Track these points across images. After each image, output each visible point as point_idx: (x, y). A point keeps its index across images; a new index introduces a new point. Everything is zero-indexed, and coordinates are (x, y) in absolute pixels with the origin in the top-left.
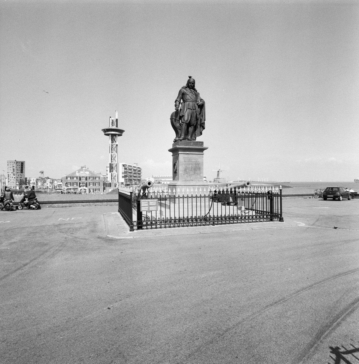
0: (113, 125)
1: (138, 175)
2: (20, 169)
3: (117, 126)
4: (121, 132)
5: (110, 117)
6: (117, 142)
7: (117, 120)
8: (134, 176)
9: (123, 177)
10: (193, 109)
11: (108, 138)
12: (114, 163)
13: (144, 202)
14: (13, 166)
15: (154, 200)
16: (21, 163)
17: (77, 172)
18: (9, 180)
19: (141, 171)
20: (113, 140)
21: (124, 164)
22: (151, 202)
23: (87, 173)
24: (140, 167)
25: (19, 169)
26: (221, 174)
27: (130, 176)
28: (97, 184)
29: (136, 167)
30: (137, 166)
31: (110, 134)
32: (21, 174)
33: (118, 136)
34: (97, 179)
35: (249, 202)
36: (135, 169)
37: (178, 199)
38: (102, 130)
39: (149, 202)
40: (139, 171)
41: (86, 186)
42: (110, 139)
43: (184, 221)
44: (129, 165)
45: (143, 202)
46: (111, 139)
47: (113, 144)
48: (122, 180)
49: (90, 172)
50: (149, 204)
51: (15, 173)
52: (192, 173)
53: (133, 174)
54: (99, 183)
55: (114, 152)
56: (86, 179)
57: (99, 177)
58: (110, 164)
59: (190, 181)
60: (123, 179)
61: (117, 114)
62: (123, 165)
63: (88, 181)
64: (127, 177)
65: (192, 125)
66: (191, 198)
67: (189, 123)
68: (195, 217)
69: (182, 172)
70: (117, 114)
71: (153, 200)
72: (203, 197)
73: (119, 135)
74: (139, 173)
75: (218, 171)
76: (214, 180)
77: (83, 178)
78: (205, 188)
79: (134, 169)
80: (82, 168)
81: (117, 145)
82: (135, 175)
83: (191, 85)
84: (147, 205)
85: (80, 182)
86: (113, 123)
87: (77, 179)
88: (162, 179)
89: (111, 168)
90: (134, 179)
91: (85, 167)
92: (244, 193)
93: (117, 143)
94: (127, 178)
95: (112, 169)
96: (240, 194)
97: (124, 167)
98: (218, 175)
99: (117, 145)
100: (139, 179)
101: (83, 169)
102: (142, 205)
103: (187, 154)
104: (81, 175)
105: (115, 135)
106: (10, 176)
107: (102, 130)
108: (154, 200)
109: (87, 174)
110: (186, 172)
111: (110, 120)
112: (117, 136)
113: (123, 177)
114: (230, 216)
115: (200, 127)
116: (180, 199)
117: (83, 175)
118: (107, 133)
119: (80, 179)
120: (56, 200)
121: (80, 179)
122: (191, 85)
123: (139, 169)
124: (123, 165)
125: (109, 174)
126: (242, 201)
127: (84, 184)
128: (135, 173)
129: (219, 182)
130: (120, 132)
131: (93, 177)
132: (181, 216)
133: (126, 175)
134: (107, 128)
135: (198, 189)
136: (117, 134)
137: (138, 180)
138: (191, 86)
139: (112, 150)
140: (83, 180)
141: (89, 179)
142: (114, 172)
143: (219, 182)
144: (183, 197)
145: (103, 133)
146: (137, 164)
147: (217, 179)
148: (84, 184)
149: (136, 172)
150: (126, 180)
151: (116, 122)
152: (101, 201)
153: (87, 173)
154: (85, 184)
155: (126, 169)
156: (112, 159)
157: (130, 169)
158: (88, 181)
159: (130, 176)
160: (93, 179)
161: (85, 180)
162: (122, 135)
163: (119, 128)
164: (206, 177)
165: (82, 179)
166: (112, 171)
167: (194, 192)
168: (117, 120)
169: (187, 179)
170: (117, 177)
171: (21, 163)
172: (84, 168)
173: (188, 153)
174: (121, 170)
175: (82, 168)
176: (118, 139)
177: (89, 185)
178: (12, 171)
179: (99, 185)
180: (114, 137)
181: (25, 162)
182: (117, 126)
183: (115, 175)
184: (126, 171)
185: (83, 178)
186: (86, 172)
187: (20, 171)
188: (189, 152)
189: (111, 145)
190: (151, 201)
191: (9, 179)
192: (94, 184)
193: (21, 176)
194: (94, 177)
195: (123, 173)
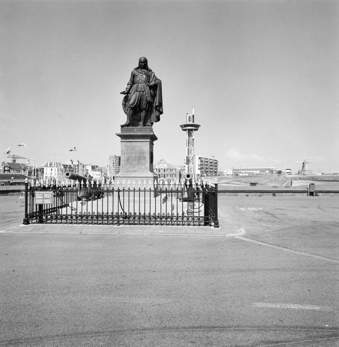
0: (190, 121)
1: (214, 167)
2: (118, 163)
3: (193, 122)
4: (197, 126)
5: (187, 114)
6: (193, 136)
7: (193, 116)
8: (210, 168)
9: (199, 169)
10: (142, 91)
11: (186, 133)
12: (191, 156)
13: (39, 194)
14: (113, 160)
15: (49, 193)
16: (119, 157)
17: (157, 164)
18: (110, 172)
19: (218, 163)
20: (190, 135)
21: (200, 156)
22: (46, 194)
23: (166, 165)
24: (216, 159)
25: (117, 162)
26: (307, 167)
27: (206, 168)
28: (174, 176)
29: (212, 160)
30: (214, 159)
31: (187, 129)
32: (119, 166)
33: (195, 131)
34: (174, 171)
35: (68, 198)
36: (212, 161)
37: (128, 192)
38: (180, 126)
39: (43, 194)
40: (216, 163)
41: (164, 177)
42: (186, 134)
43: (102, 218)
44: (205, 158)
45: (37, 194)
46: (188, 134)
47: (189, 138)
48: (198, 172)
49: (168, 165)
50: (44, 196)
51: (114, 166)
52: (135, 163)
53: (210, 167)
54: (176, 174)
55: (191, 146)
56: (164, 171)
57: (176, 169)
58: (187, 157)
59: (132, 171)
60: (200, 171)
61: (193, 110)
62: (200, 158)
63: (166, 173)
64: (203, 169)
65: (143, 110)
66: (133, 192)
67: (143, 108)
68: (117, 213)
69: (123, 162)
70: (193, 110)
71: (48, 193)
72: (122, 191)
73: (195, 130)
74: (216, 165)
75: (304, 163)
76: (299, 173)
77: (162, 170)
78: (134, 180)
79: (210, 161)
80: (161, 160)
81: (193, 139)
82: (211, 167)
83: (143, 65)
84: (42, 197)
85: (159, 173)
86: (190, 119)
87: (157, 171)
88: (242, 171)
89: (188, 161)
90: (210, 171)
91: (164, 160)
92: (71, 186)
93: (193, 137)
94: (203, 170)
95: (189, 162)
96: (71, 188)
97: (200, 160)
98: (303, 167)
99: (193, 139)
100: (215, 171)
101: (162, 162)
102: (37, 197)
103: (130, 142)
104: (160, 168)
105: (192, 130)
106: (111, 168)
107: (180, 126)
108: (49, 193)
109: (165, 166)
110: (128, 162)
111: (188, 116)
112: (193, 130)
113: (199, 169)
114: (157, 215)
115: (156, 111)
116: (140, 192)
117: (162, 167)
118: (184, 128)
119: (159, 171)
120: (329, 190)
121: (159, 171)
122: (143, 65)
123: (216, 162)
124: (200, 158)
125: (187, 166)
126: (153, 198)
127: (163, 175)
128: (211, 166)
129: (304, 175)
130: (194, 127)
131: (170, 169)
132: (100, 211)
133: (202, 167)
134: (185, 124)
135: (142, 182)
136: (193, 129)
137: (215, 172)
138: (142, 66)
139: (189, 144)
140: (162, 172)
141: (167, 171)
142: (191, 164)
143: (304, 175)
144: (134, 190)
145: (181, 129)
146: (214, 157)
147: (302, 172)
148: (161, 176)
149: (213, 164)
150: (202, 172)
151: (192, 118)
152: (300, 192)
153: (166, 165)
154: (163, 176)
155: (202, 161)
156: (189, 152)
157: (206, 162)
158: (166, 173)
159: (206, 168)
160: (170, 171)
161: (163, 172)
162: (198, 130)
163: (196, 123)
164: (290, 169)
165: (161, 171)
166: (189, 164)
167: (131, 184)
168: (193, 116)
169: (129, 170)
170: (193, 169)
171: (119, 157)
172: (163, 161)
173: (131, 140)
174: (197, 162)
175: (161, 160)
176: (194, 133)
177: (167, 176)
178: (112, 164)
179: (176, 177)
180: (191, 132)
181: (199, 157)
182: (193, 122)
183: (191, 167)
184: (202, 163)
185: (162, 170)
186: (164, 165)
187: (118, 164)
188: (126, 139)
189: (188, 140)
190: (45, 194)
191: (110, 171)
192: (171, 175)
193: (119, 168)
194: (171, 169)
195: (199, 165)
